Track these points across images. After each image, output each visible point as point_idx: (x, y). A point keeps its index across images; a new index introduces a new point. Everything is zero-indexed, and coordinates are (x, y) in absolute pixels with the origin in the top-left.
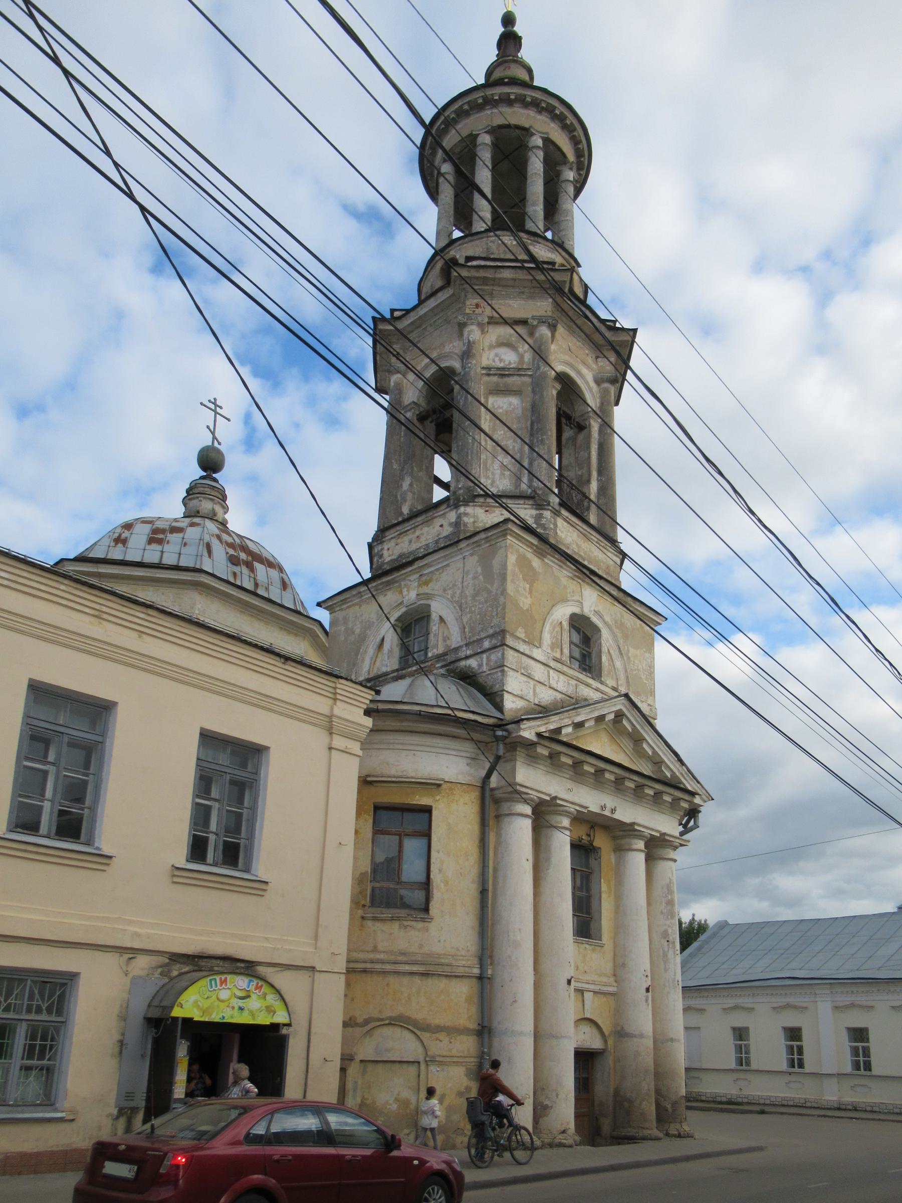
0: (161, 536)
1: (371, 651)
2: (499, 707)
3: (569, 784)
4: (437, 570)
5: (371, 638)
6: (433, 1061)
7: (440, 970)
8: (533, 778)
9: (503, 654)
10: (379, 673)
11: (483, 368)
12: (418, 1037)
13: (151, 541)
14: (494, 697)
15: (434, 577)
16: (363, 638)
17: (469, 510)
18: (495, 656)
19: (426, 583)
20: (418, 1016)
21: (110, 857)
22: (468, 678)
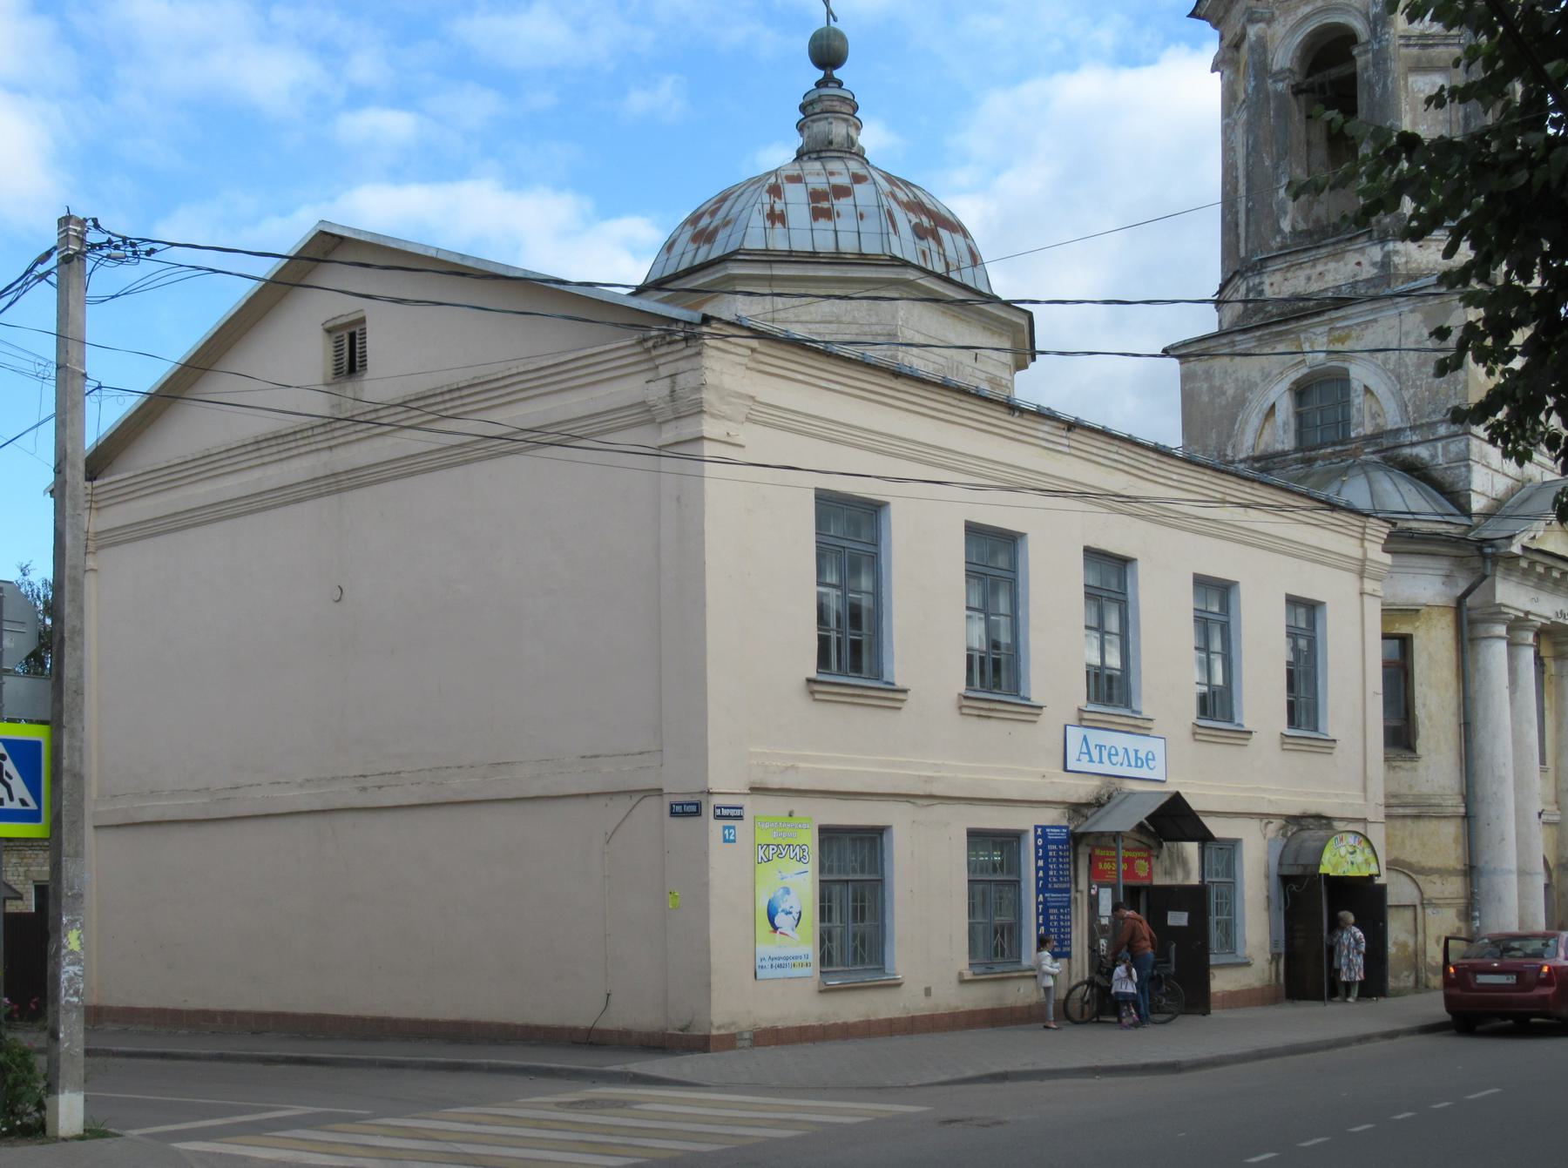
0: (825, 205)
1: (1255, 421)
2: (1465, 510)
3: (1533, 593)
4: (1358, 324)
5: (1255, 403)
6: (1430, 904)
7: (1431, 811)
8: (1511, 594)
9: (1468, 446)
10: (1270, 450)
11: (1401, 37)
12: (1414, 881)
13: (817, 214)
14: (1456, 497)
15: (1354, 334)
16: (1240, 402)
17: (1399, 246)
18: (1455, 447)
19: (1342, 340)
20: (1413, 859)
21: (904, 691)
22: (1416, 471)
